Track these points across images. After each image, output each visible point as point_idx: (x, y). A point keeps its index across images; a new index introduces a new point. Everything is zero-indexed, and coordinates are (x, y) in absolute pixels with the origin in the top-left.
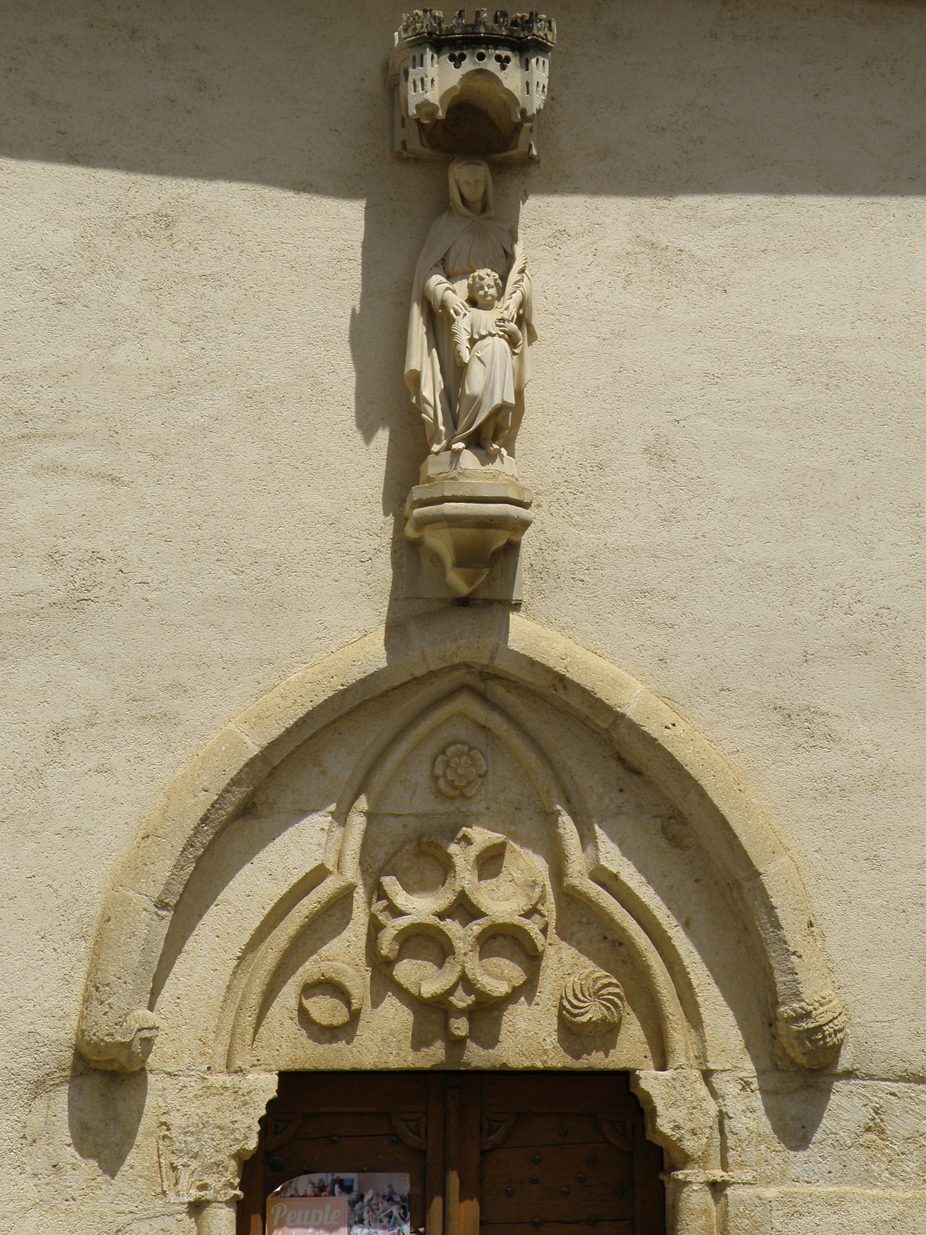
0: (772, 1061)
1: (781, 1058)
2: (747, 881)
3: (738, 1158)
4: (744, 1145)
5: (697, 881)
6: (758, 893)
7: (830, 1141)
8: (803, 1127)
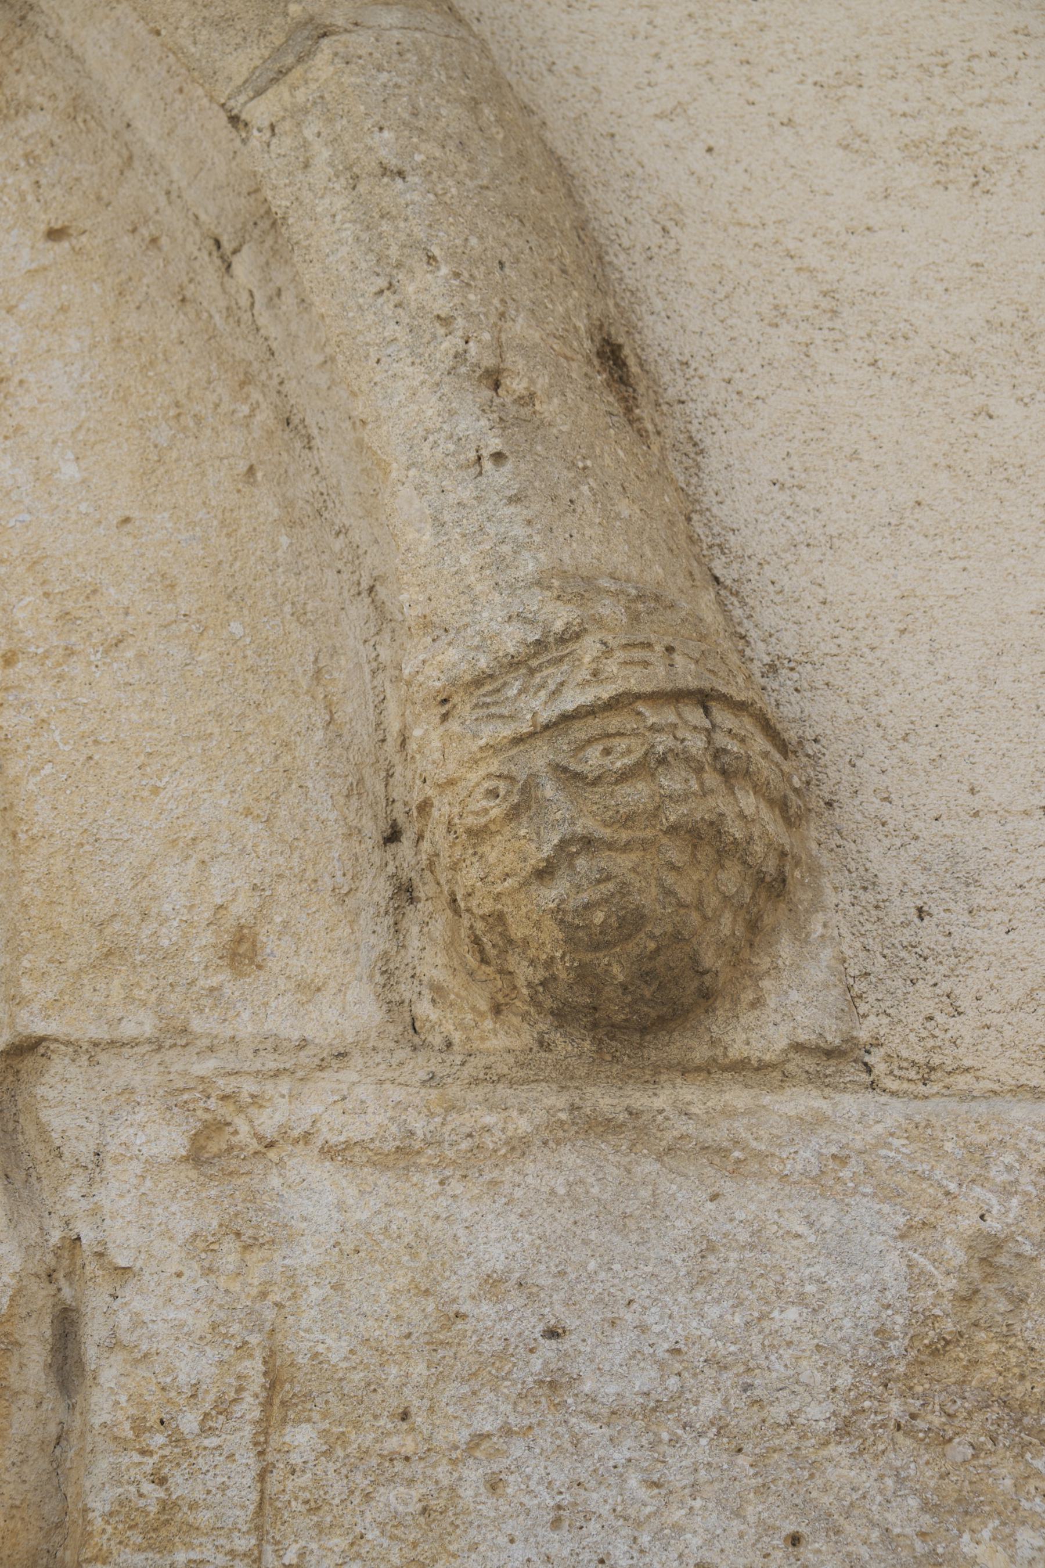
0: (393, 1007)
1: (438, 991)
2: (259, 93)
3: (147, 1487)
4: (189, 1422)
5: (55, 234)
6: (309, 133)
7: (709, 1405)
8: (552, 1333)
